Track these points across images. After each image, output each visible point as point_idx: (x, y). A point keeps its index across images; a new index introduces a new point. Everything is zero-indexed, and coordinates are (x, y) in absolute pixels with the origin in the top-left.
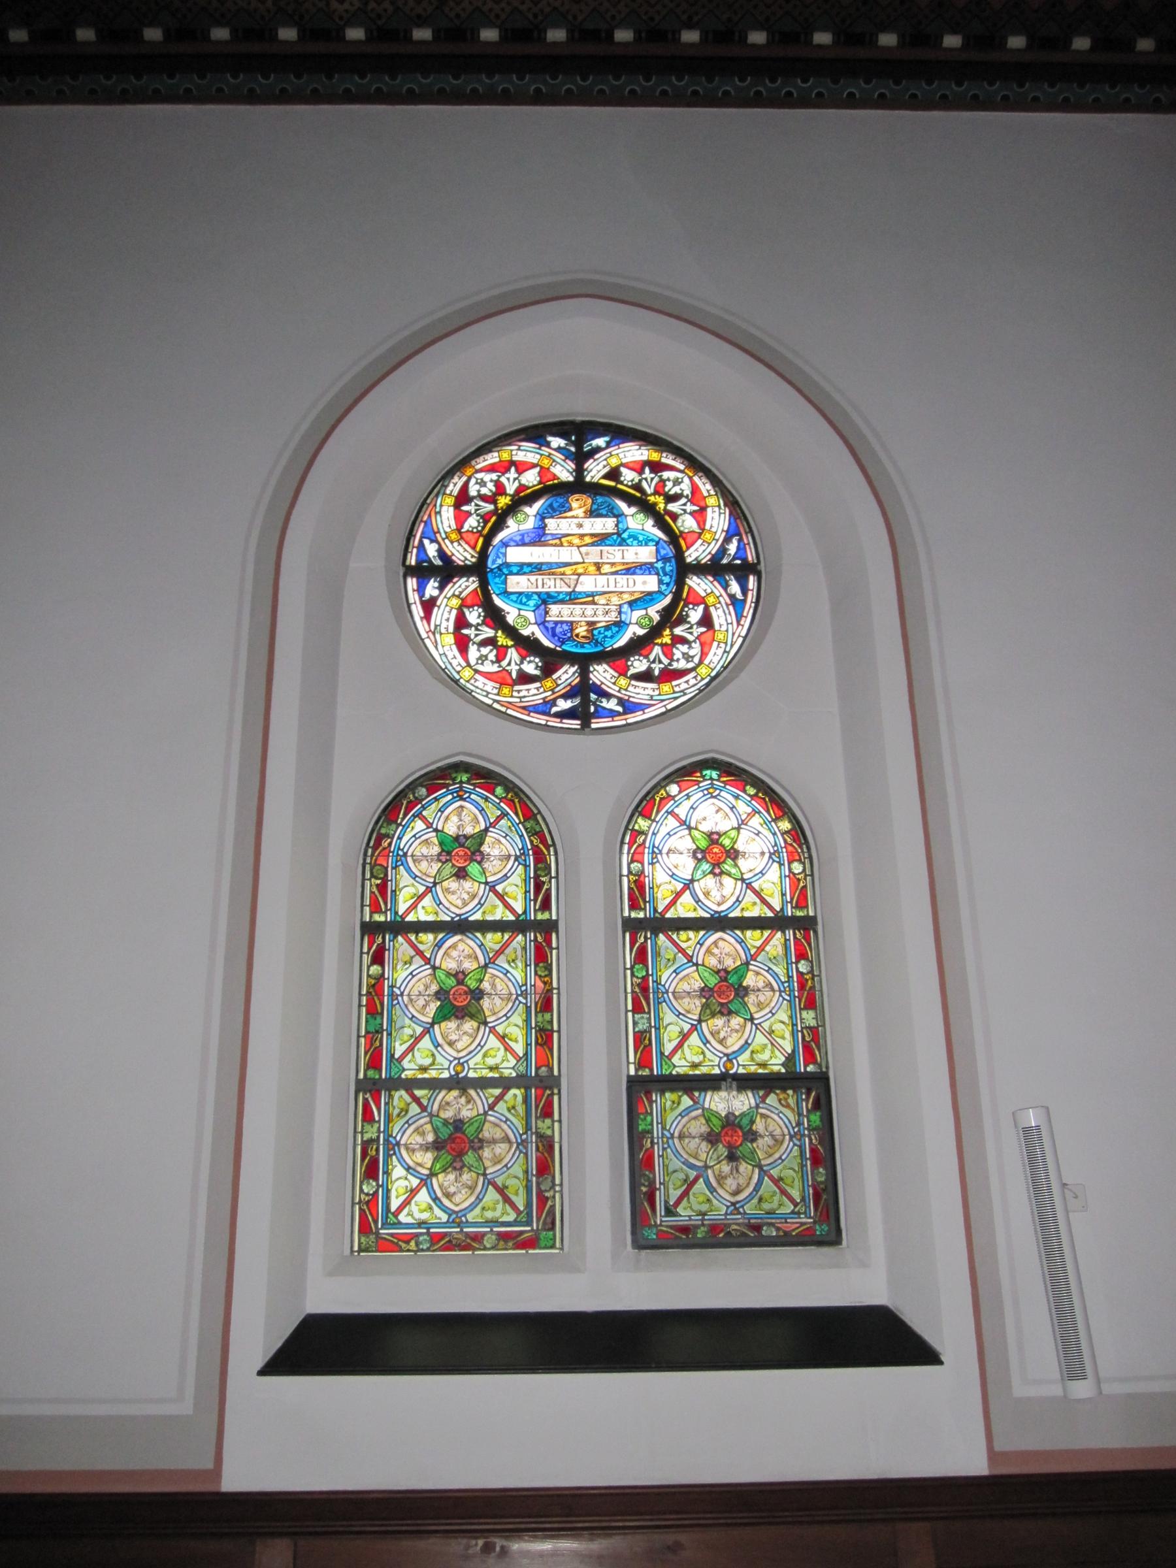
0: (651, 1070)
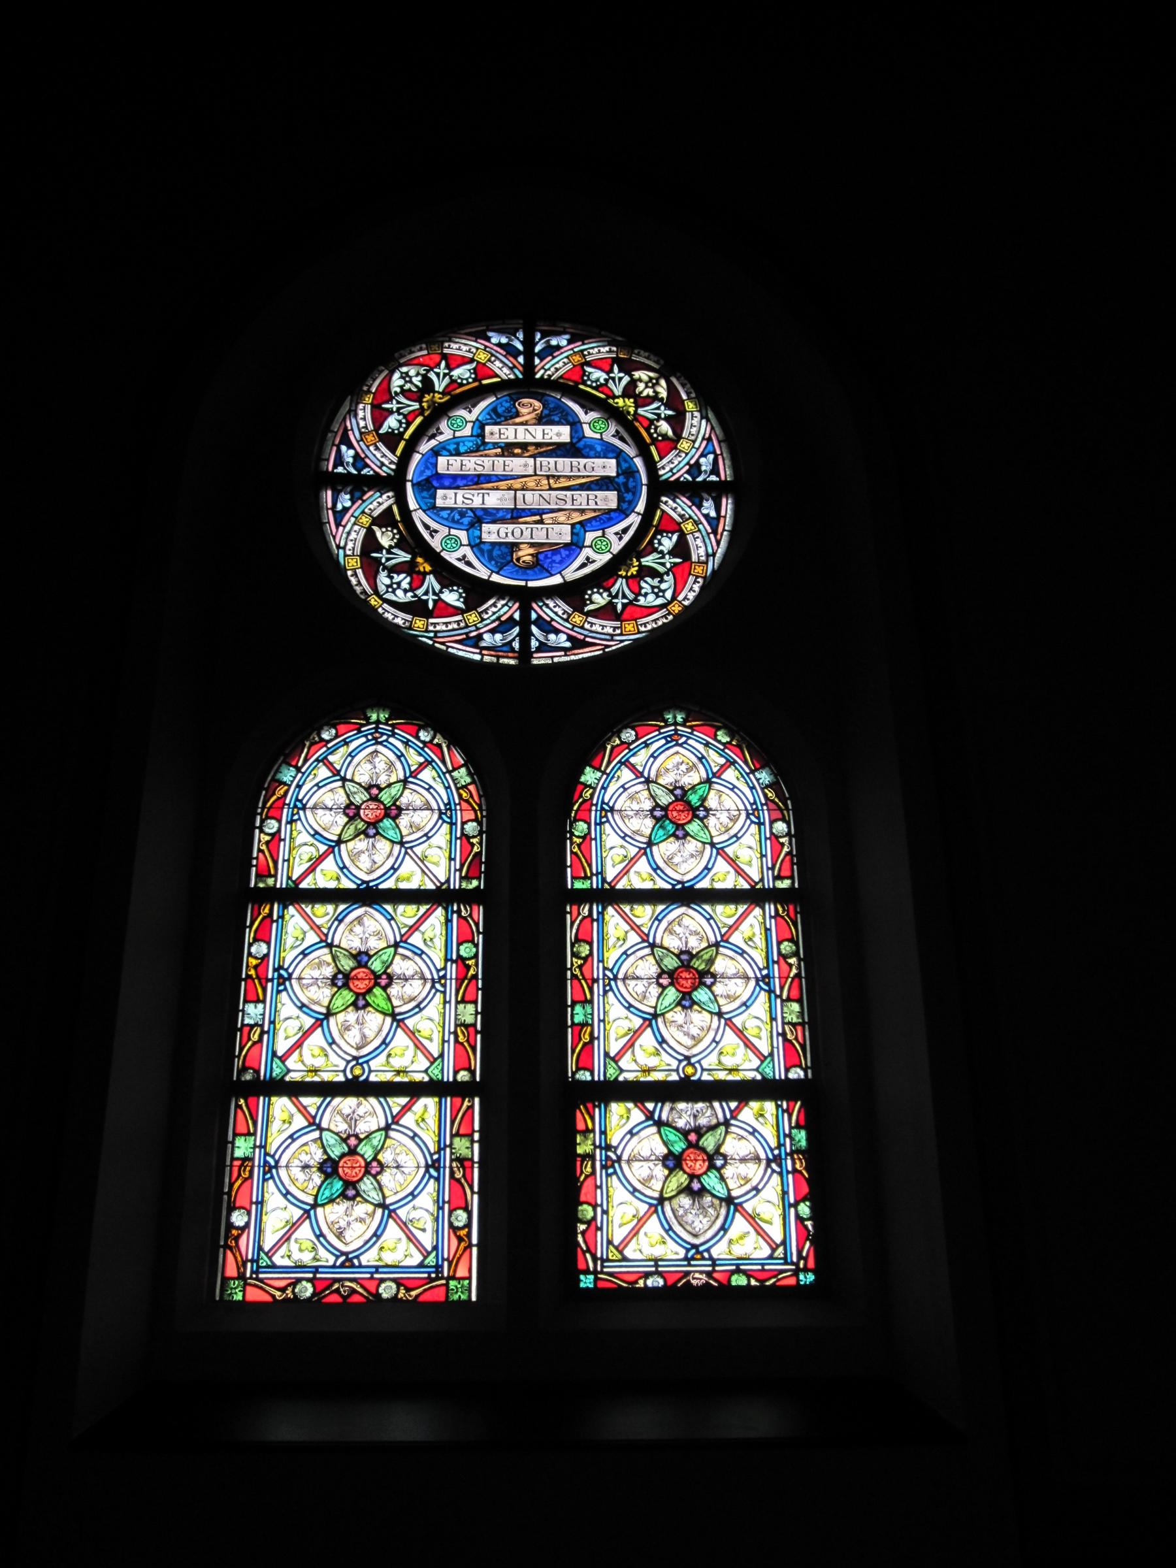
0: (592, 1074)
